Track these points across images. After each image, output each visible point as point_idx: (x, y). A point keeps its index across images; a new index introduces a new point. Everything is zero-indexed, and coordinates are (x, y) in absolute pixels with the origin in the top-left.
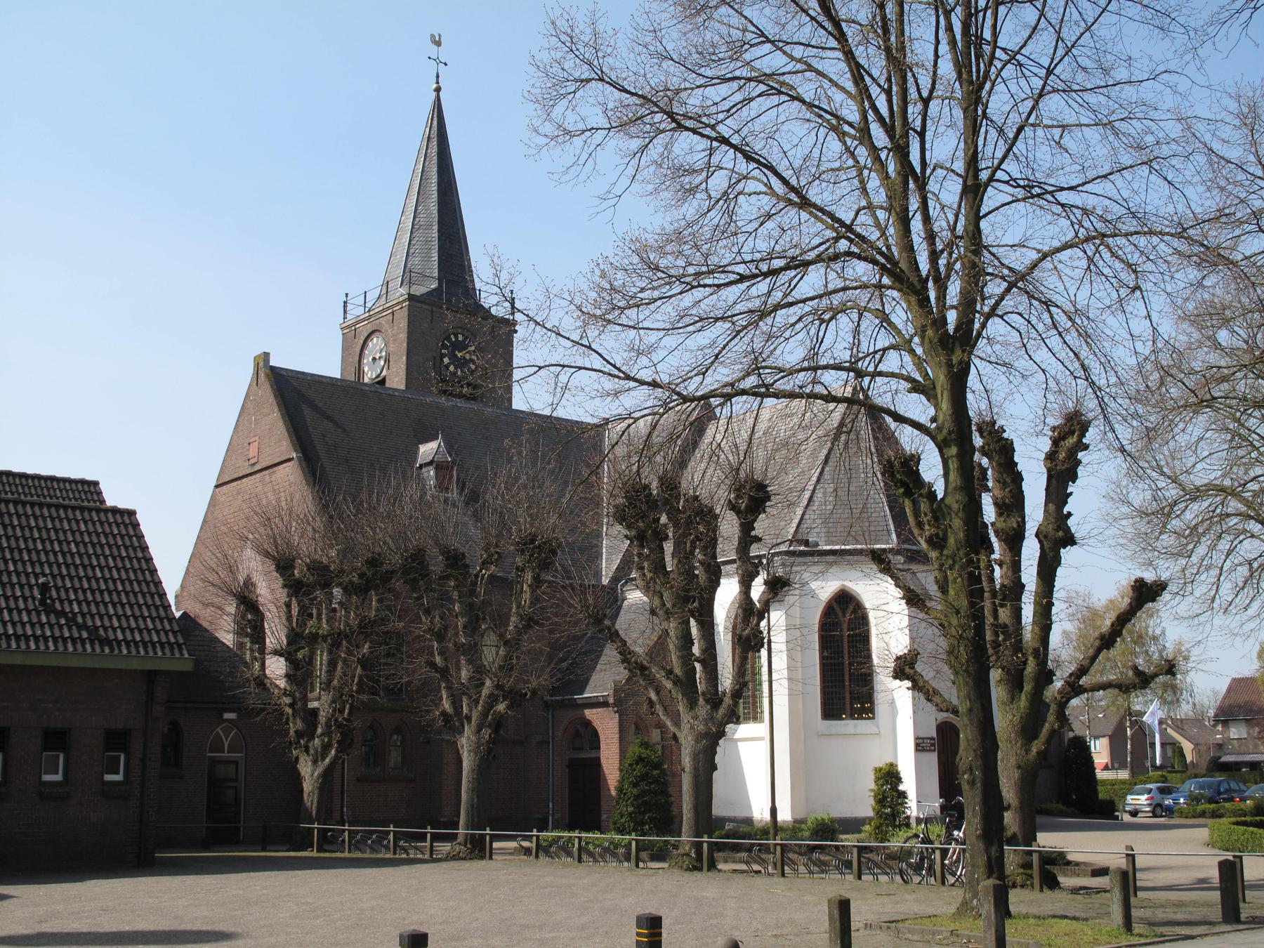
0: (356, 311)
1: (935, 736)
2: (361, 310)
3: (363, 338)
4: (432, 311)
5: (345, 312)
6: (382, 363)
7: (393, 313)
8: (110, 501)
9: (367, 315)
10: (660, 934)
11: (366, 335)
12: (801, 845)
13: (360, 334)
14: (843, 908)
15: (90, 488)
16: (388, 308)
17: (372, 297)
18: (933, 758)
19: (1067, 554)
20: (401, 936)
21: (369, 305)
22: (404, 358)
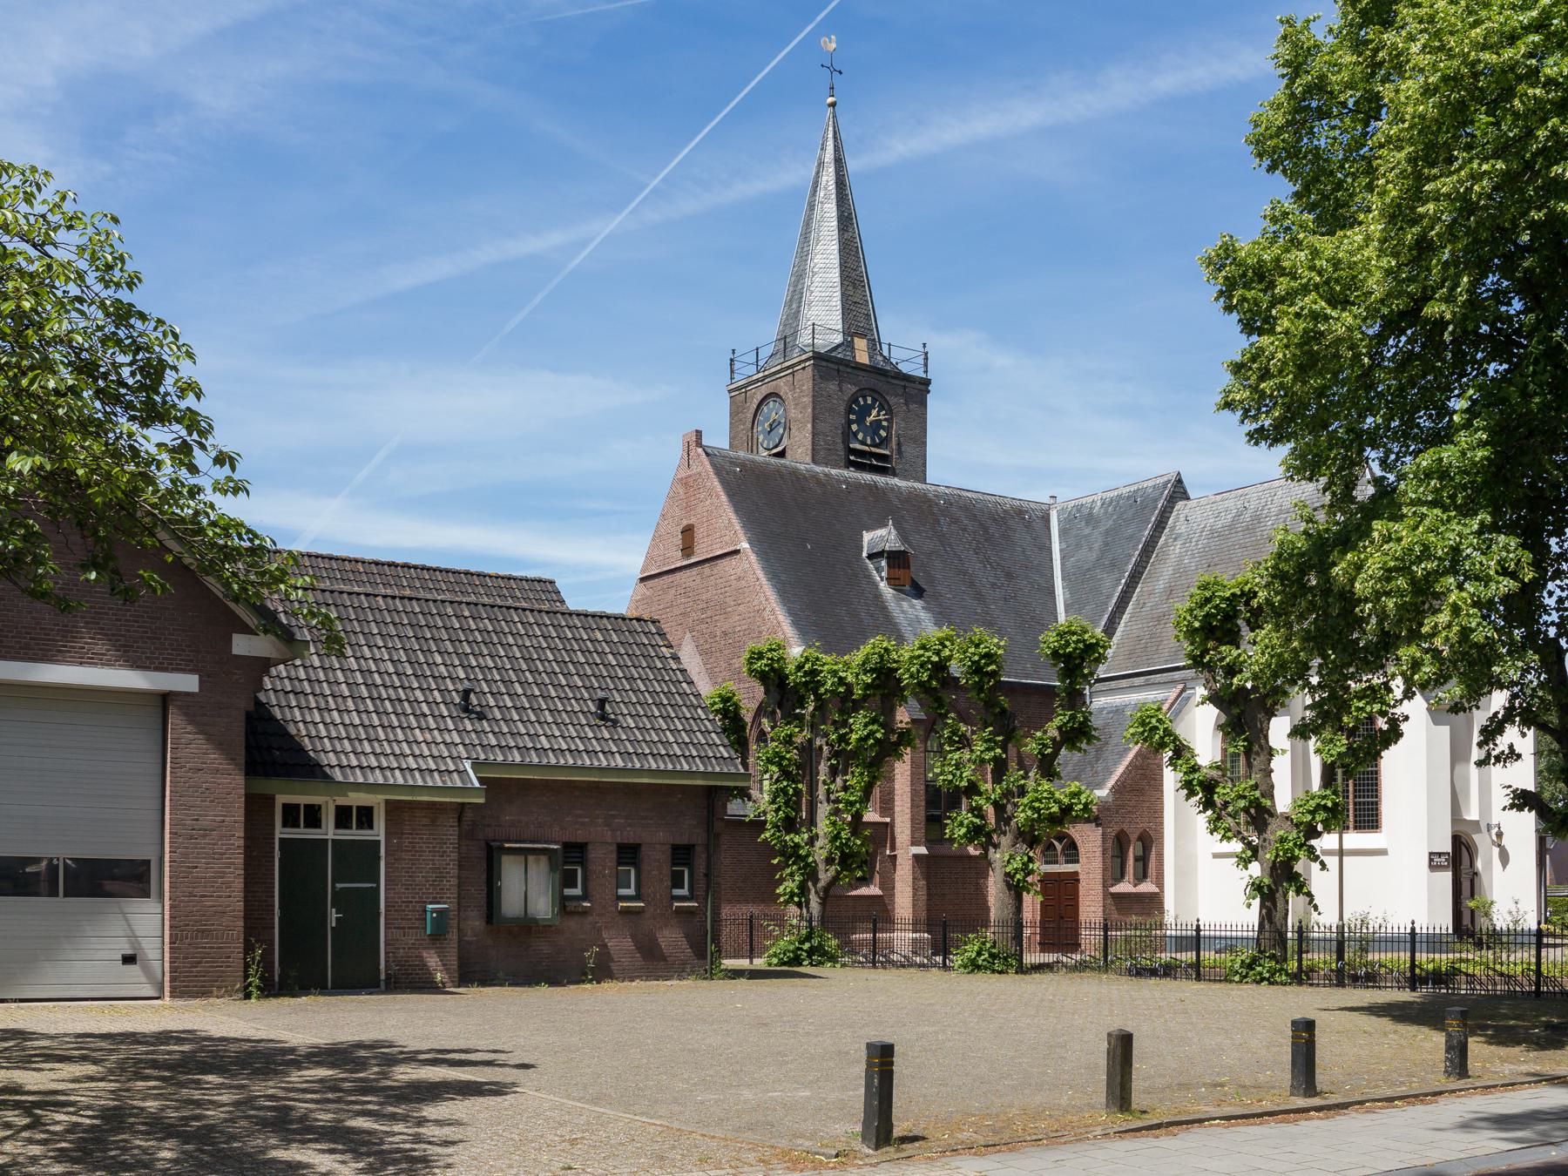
0: (746, 371)
1: (1450, 850)
2: (753, 369)
3: (756, 402)
4: (838, 371)
5: (732, 372)
6: (781, 431)
7: (793, 373)
8: (573, 604)
9: (761, 375)
10: (892, 1063)
11: (760, 398)
12: (386, 953)
13: (752, 397)
14: (1304, 1032)
15: (546, 587)
16: (788, 368)
17: (765, 353)
18: (1446, 877)
19: (1180, 505)
20: (1109, 1035)
21: (761, 363)
22: (809, 426)
